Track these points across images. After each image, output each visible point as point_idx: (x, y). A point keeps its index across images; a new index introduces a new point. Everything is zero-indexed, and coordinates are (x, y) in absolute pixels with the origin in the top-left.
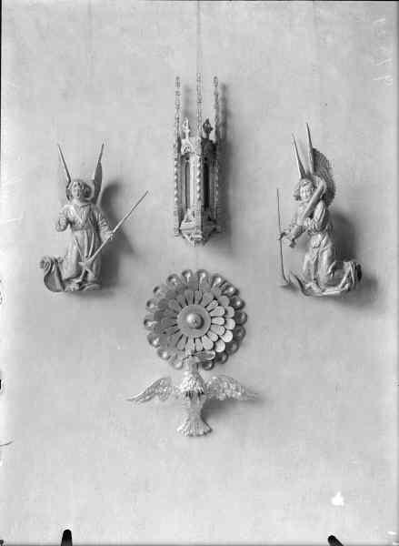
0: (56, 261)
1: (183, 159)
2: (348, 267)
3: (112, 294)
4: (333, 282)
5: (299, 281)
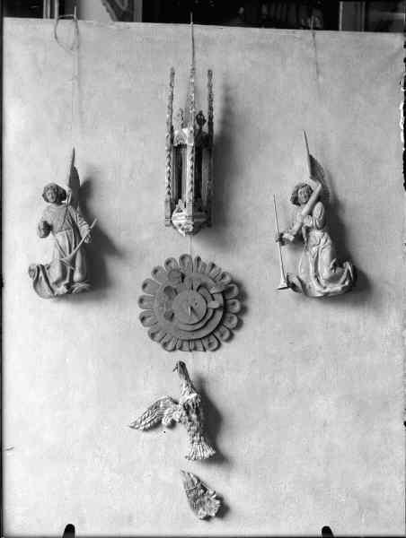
0: (43, 267)
1: (177, 150)
2: (348, 267)
3: (105, 296)
4: (333, 279)
5: (300, 280)
